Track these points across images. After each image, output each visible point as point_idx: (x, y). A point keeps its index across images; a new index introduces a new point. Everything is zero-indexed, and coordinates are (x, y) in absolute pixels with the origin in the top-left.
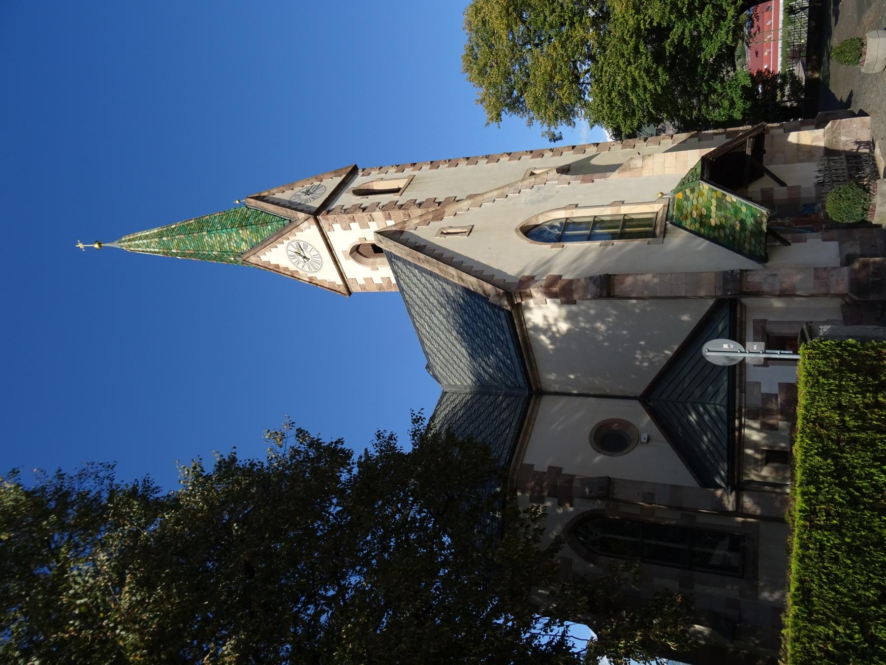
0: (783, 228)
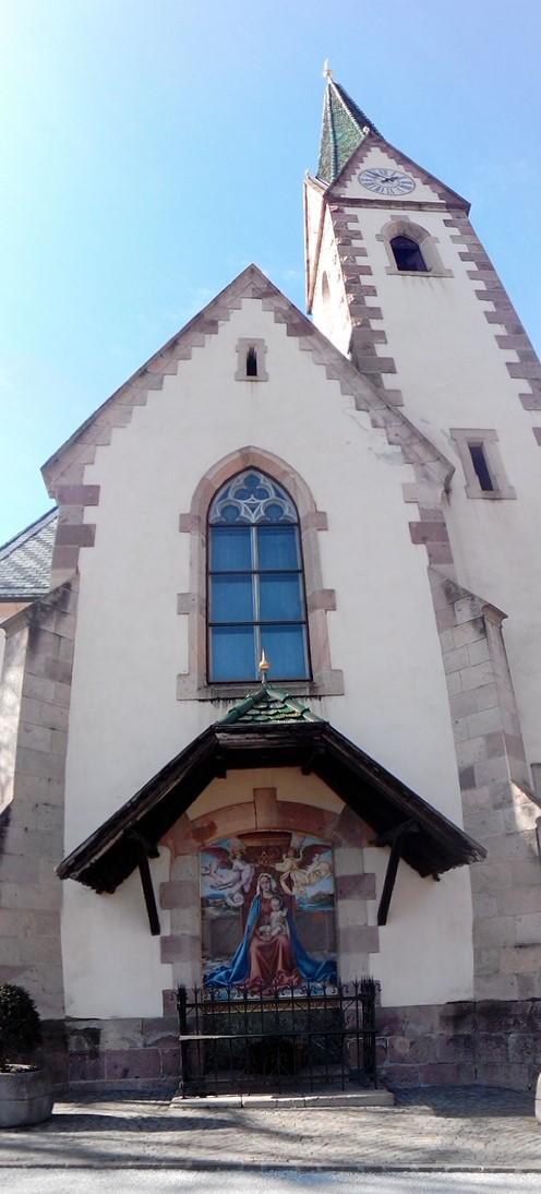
0: (249, 922)
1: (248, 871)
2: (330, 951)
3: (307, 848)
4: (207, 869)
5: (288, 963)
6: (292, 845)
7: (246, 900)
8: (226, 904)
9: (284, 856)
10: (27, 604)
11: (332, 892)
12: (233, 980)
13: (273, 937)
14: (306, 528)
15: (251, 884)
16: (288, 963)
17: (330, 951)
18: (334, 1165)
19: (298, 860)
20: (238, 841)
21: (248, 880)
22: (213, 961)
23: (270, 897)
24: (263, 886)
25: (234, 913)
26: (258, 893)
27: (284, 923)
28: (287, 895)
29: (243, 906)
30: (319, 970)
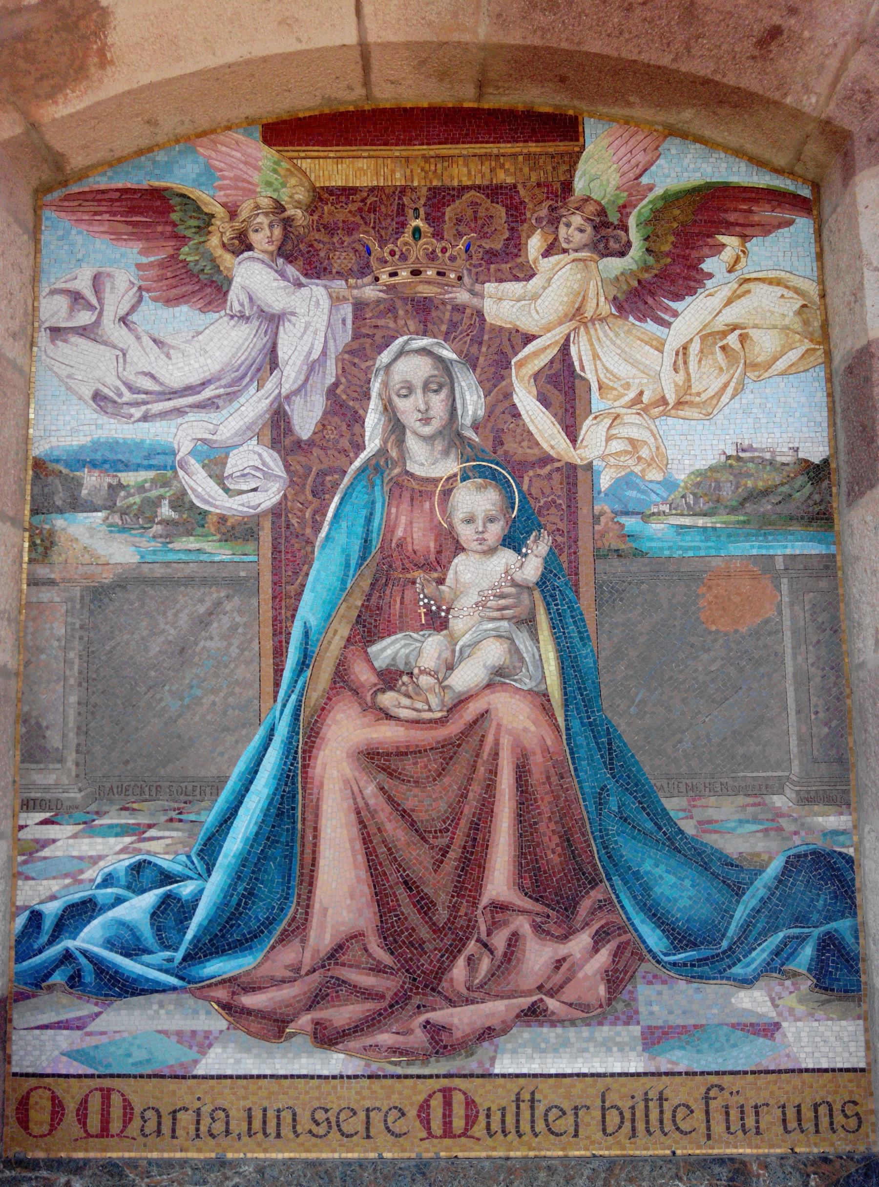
1: (320, 321)
2: (806, 800)
3: (671, 200)
4: (76, 297)
5: (553, 857)
6: (579, 185)
7: (295, 479)
8: (180, 501)
9: (535, 244)
10: (146, 835)
11: (817, 453)
12: (193, 957)
13: (462, 701)
14: (797, 1059)
15: (331, 392)
16: (553, 857)
17: (806, 800)
18: (206, 497)
19: (614, 265)
20: (266, 155)
21: (313, 367)
22: (89, 828)
23: (451, 466)
24: (407, 408)
25: (223, 553)
26: (373, 444)
27: (528, 622)
28: (546, 460)
29: (276, 512)
30: (741, 913)
